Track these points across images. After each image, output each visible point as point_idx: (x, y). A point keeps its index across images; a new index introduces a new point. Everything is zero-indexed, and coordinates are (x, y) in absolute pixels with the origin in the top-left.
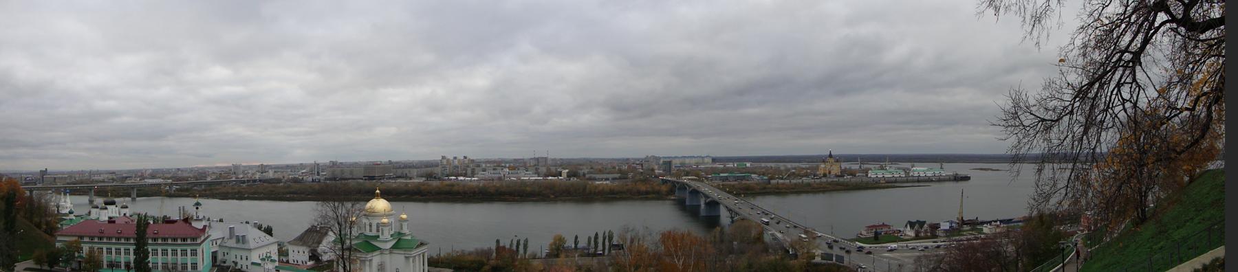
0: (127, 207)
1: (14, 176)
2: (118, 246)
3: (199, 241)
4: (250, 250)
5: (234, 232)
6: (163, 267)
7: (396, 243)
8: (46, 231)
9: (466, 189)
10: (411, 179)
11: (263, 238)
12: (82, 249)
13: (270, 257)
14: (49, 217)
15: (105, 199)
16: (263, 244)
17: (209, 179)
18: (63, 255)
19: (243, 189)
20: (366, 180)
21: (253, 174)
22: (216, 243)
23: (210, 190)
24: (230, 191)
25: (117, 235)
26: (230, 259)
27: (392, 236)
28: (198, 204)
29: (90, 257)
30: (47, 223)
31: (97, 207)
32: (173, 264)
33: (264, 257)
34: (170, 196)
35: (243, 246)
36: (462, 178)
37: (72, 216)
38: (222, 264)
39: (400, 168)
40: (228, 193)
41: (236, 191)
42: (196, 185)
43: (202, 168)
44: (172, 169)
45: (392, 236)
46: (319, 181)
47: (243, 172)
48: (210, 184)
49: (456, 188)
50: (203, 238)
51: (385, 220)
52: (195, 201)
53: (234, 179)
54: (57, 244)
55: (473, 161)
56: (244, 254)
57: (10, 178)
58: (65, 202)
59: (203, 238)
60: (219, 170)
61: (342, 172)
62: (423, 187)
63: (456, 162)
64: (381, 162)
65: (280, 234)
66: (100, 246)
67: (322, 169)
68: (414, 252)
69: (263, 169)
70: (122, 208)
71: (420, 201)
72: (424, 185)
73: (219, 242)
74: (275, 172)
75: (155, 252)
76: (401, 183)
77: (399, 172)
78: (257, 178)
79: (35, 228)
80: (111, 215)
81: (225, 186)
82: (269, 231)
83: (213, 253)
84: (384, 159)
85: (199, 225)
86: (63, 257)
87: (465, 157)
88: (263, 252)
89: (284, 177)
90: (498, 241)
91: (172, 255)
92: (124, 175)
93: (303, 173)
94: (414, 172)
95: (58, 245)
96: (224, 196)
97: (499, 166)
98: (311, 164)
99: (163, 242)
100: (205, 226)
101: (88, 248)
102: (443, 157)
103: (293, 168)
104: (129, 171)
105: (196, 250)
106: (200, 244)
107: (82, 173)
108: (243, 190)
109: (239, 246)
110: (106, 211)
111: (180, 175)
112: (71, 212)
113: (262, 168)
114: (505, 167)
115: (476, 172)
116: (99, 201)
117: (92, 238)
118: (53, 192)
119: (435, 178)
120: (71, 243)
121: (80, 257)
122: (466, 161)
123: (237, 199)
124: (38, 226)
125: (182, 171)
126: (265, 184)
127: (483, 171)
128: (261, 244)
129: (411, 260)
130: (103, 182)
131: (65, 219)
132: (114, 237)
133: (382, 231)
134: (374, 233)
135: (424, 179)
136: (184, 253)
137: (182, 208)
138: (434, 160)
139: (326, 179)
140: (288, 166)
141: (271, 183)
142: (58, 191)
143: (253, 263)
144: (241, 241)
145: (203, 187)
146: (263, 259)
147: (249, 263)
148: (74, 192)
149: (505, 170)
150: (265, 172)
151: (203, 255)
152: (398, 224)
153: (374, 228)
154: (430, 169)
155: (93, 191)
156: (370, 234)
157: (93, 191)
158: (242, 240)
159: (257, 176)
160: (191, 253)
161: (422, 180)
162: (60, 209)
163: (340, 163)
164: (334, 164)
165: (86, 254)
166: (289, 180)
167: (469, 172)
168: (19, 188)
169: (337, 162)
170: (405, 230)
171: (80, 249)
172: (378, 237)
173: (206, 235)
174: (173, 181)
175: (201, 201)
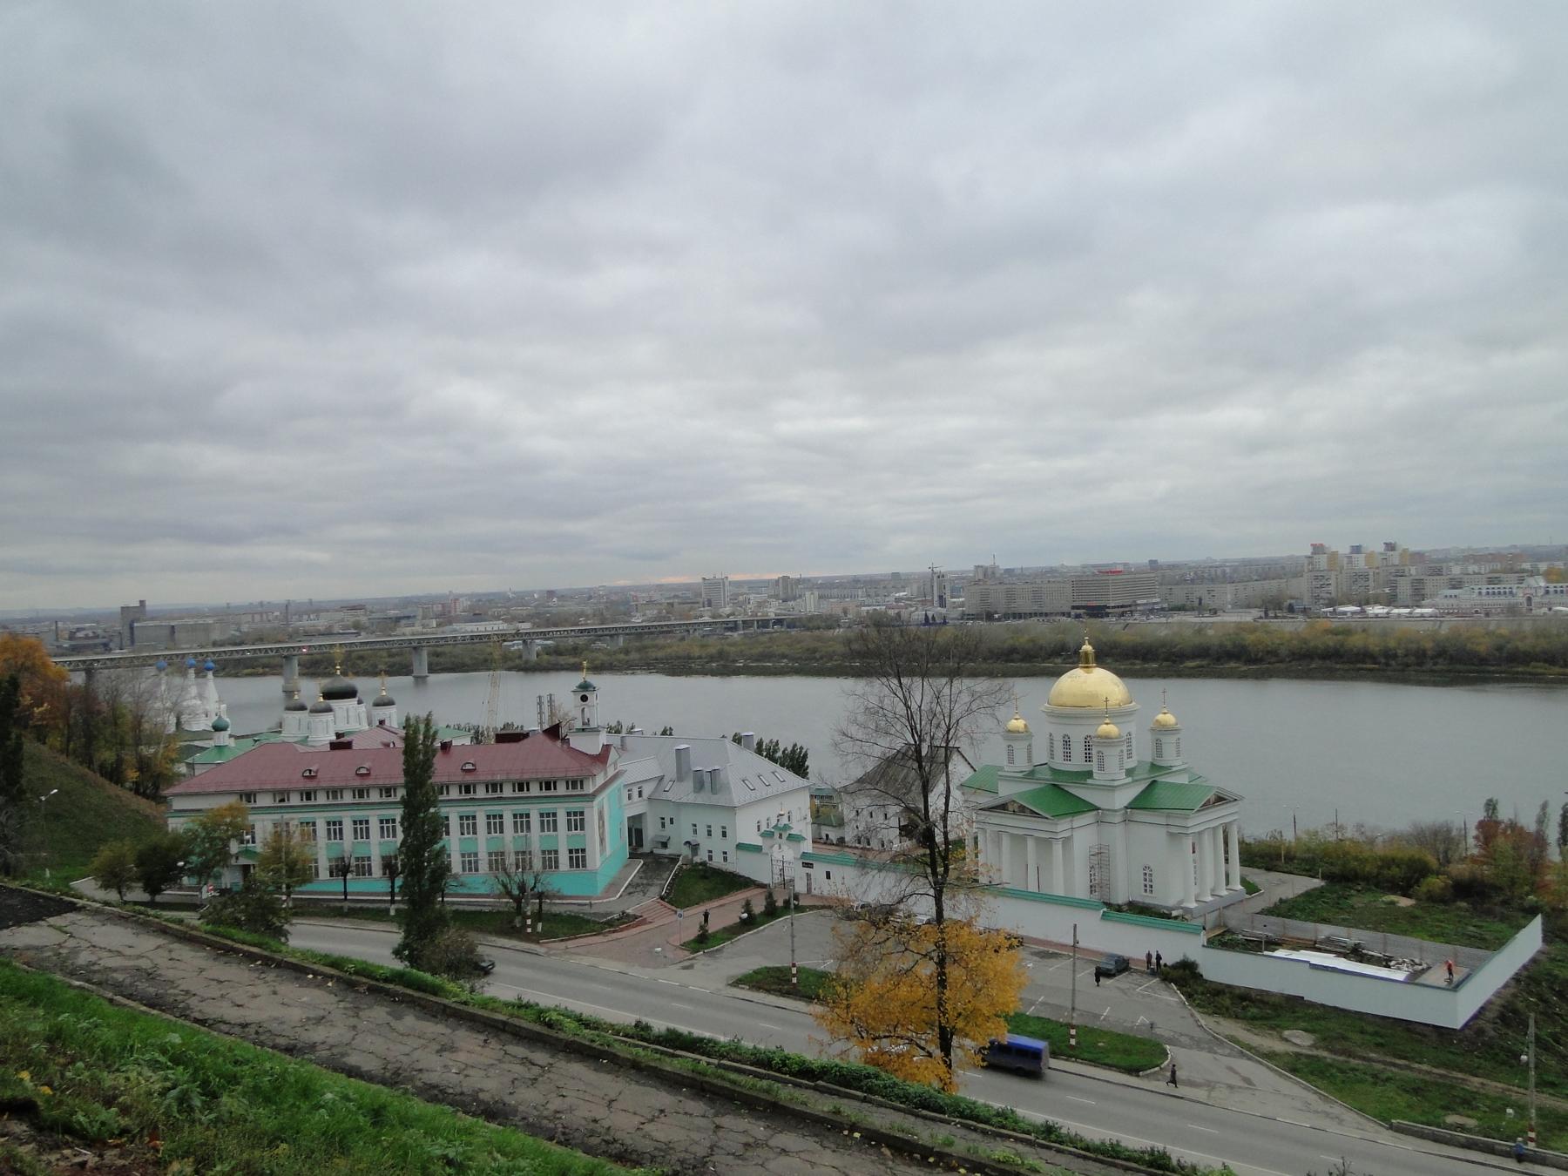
0: (391, 703)
1: (19, 628)
2: (360, 814)
3: (590, 788)
7: (1147, 788)
8: (138, 789)
9: (1392, 644)
10: (1214, 612)
12: (251, 830)
13: (786, 827)
14: (149, 744)
15: (325, 682)
16: (770, 791)
17: (637, 620)
18: (191, 853)
19: (734, 644)
20: (1078, 616)
21: (760, 605)
22: (640, 794)
24: (696, 652)
25: (357, 783)
26: (679, 837)
28: (585, 691)
29: (277, 850)
30: (143, 765)
31: (302, 708)
32: (517, 853)
36: (1378, 610)
37: (223, 738)
41: (713, 650)
43: (624, 589)
44: (531, 594)
45: (1129, 772)
47: (734, 597)
48: (639, 633)
49: (1356, 641)
50: (600, 780)
52: (577, 678)
53: (706, 619)
54: (170, 821)
55: (1418, 557)
57: (14, 636)
58: (201, 696)
59: (600, 780)
61: (1010, 595)
62: (1250, 638)
63: (1360, 562)
65: (829, 769)
66: (308, 816)
67: (952, 590)
69: (788, 588)
70: (377, 705)
72: (1254, 630)
73: (647, 792)
74: (820, 597)
75: (468, 822)
77: (1179, 596)
78: (772, 616)
79: (102, 780)
80: (342, 728)
81: (683, 639)
82: (796, 763)
83: (632, 819)
84: (1137, 557)
86: (194, 858)
87: (1391, 547)
88: (768, 814)
89: (845, 613)
90: (1491, 806)
92: (393, 613)
93: (898, 600)
94: (1228, 593)
95: (176, 825)
96: (679, 666)
97: (1512, 571)
100: (607, 748)
101: (270, 827)
102: (1318, 549)
103: (871, 585)
104: (407, 602)
105: (582, 813)
106: (594, 795)
107: (262, 609)
109: (701, 798)
110: (329, 717)
112: (218, 728)
113: (785, 588)
114: (1532, 573)
115: (1427, 591)
116: (310, 689)
117: (282, 795)
118: (160, 669)
119: (1291, 609)
120: (217, 815)
121: (247, 853)
122: (1395, 558)
123: (713, 673)
124: (114, 774)
125: (562, 597)
126: (794, 632)
127: (1454, 587)
128: (762, 792)
129: (1188, 842)
130: (328, 633)
131: (203, 749)
132: (346, 788)
134: (1077, 763)
135: (1256, 613)
136: (549, 820)
138: (1291, 558)
139: (963, 616)
140: (856, 582)
141: (808, 629)
142: (177, 665)
143: (740, 847)
144: (707, 785)
145: (621, 641)
146: (768, 835)
148: (232, 666)
149: (1531, 581)
150: (794, 599)
151: (602, 826)
153: (1078, 750)
155: (295, 662)
157: (295, 662)
158: (708, 782)
159: (772, 611)
160: (569, 821)
161: (1248, 617)
162: (184, 718)
163: (1008, 571)
164: (987, 575)
165: (266, 844)
167: (1404, 588)
168: (45, 665)
169: (994, 568)
171: (240, 831)
172: (1089, 774)
173: (611, 772)
174: (534, 624)
175: (594, 679)
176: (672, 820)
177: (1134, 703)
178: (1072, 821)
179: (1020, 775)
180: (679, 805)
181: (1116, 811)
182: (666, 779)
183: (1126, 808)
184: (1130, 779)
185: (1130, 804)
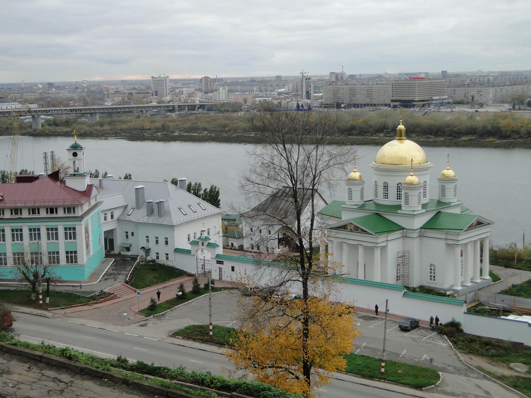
4: (172, 227)
5: (143, 196)
6: (14, 260)
11: (195, 207)
13: (206, 239)
16: (196, 216)
17: (108, 104)
19: (173, 121)
20: (395, 107)
21: (190, 95)
22: (112, 217)
23: (110, 123)
24: (147, 125)
27: (424, 206)
33: (196, 240)
34: (36, 134)
35: (160, 221)
38: (123, 253)
39: (463, 85)
40: (143, 129)
41: (159, 125)
42: (83, 113)
45: (424, 206)
46: (310, 109)
47: (172, 90)
48: (110, 112)
50: (86, 208)
51: (412, 179)
52: (70, 142)
53: (154, 104)
56: (162, 235)
59: (86, 208)
60: (128, 87)
61: (352, 92)
62: (502, 123)
64: (427, 74)
67: (315, 88)
68: (465, 237)
71: (497, 146)
72: (505, 118)
73: (117, 214)
74: (230, 91)
76: (460, 112)
77: (460, 94)
78: (197, 103)
85: (80, 185)
88: (195, 230)
91: (66, 238)
93: (280, 94)
94: (490, 93)
98: (295, 79)
99: (14, 216)
100: (90, 187)
105: (74, 229)
106: (81, 218)
108: (171, 124)
111: (53, 96)
113: (206, 84)
123: (159, 140)
125: (58, 87)
126: (212, 113)
128: (191, 216)
129: (458, 250)
132: (25, 207)
133: (407, 197)
134: (392, 200)
137: (49, 155)
140: (253, 81)
141: (221, 112)
143: (177, 250)
145: (98, 118)
146: (194, 243)
147: (169, 250)
150: (212, 91)
151: (87, 237)
152: (437, 185)
153: (392, 192)
154: (520, 87)
156: (385, 202)
159: (197, 99)
164: (337, 78)
166: (254, 107)
169: (342, 74)
170: (450, 197)
172: (399, 207)
173: (93, 202)
174: (40, 106)
175: (81, 142)
176: (133, 234)
177: (429, 163)
178: (387, 236)
179: (356, 207)
180: (138, 224)
181: (415, 230)
182: (129, 208)
183: (421, 228)
184: (424, 211)
185: (424, 225)
